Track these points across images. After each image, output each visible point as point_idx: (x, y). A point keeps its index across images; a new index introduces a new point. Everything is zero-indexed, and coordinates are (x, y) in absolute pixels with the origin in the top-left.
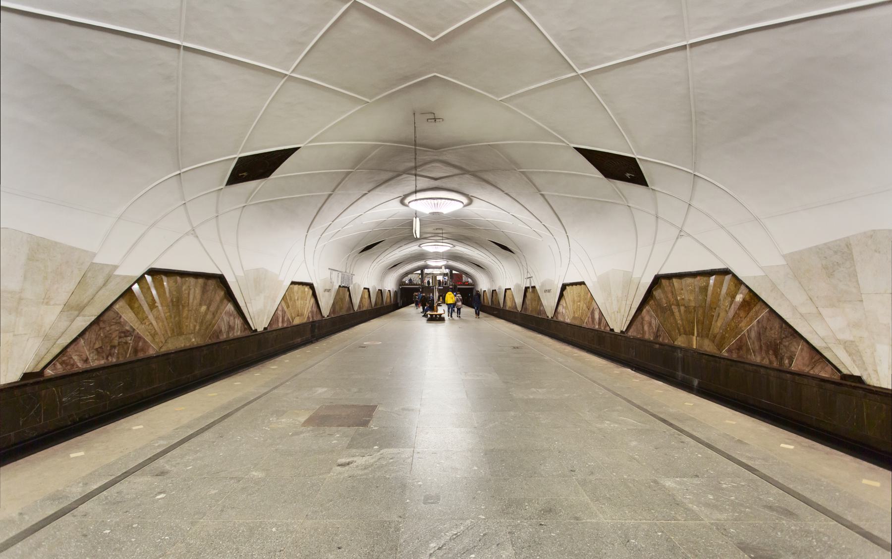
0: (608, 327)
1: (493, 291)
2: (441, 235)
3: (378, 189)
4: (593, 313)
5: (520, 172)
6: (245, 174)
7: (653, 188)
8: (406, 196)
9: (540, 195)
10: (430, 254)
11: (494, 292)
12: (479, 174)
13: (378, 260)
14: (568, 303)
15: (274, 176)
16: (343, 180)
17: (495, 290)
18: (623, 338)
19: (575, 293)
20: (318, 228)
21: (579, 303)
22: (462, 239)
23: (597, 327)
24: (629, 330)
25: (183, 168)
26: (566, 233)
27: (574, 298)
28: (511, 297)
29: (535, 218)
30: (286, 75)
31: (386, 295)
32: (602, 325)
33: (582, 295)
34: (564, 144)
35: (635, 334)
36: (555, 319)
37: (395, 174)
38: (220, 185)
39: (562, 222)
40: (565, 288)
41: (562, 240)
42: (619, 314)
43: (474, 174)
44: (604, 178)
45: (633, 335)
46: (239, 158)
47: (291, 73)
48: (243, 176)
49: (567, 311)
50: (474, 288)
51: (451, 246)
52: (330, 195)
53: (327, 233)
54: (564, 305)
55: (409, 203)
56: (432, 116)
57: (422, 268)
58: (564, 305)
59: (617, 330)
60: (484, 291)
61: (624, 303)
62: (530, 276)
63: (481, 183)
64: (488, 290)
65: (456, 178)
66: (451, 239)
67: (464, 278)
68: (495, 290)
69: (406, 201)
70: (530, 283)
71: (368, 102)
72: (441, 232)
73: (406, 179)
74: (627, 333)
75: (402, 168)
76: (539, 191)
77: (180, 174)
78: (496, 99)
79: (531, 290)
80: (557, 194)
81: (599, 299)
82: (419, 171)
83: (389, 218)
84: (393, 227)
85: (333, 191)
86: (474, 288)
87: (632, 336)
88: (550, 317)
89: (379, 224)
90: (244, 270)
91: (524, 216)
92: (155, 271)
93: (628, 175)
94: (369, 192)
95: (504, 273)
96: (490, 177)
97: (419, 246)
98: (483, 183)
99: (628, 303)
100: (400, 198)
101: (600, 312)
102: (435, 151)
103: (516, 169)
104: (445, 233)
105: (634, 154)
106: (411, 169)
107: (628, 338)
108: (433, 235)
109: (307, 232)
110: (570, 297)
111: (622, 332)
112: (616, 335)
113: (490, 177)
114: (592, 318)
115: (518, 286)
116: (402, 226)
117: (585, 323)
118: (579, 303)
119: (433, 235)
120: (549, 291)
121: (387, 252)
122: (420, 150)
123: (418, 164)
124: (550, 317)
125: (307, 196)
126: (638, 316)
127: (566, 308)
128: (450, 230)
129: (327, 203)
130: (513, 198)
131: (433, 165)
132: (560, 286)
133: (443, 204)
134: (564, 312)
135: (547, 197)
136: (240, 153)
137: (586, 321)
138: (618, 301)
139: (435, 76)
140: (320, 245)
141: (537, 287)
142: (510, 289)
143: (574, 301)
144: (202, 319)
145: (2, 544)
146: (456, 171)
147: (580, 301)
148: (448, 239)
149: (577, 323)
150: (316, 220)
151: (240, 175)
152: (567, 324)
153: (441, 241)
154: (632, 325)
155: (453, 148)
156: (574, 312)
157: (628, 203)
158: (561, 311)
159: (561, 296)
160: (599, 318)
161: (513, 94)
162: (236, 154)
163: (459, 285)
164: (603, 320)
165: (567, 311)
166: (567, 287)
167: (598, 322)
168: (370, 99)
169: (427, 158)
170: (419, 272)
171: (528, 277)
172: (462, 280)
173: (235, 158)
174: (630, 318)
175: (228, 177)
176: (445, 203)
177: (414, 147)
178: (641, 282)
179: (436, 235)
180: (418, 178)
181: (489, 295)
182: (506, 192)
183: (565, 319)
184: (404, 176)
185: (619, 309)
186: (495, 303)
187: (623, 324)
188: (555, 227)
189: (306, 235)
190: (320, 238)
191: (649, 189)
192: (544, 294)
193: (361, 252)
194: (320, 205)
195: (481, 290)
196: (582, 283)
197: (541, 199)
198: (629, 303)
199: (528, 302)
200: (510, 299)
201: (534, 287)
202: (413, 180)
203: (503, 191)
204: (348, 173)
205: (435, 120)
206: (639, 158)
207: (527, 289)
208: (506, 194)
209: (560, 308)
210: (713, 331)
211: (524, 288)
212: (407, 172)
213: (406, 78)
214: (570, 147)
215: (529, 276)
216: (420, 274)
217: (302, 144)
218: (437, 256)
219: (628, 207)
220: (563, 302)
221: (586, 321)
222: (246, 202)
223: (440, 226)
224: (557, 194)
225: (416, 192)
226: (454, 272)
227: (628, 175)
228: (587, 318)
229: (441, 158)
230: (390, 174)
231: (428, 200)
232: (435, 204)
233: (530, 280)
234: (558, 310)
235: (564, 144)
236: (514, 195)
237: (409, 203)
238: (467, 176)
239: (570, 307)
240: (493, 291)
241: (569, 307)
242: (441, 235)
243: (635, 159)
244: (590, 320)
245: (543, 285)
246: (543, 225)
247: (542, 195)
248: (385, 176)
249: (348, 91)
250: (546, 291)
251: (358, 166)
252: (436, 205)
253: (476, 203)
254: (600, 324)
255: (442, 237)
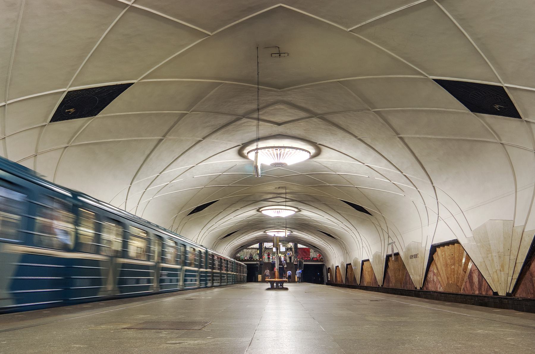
0: (491, 291)
1: (347, 265)
2: (284, 196)
3: (214, 136)
4: (471, 276)
5: (374, 111)
6: (72, 110)
7: (527, 119)
8: (245, 145)
9: (398, 139)
10: (271, 221)
11: (349, 266)
12: (329, 117)
13: (209, 226)
14: (439, 267)
15: (99, 115)
16: (176, 123)
17: (350, 264)
18: (510, 302)
19: (447, 255)
20: (143, 180)
21: (453, 267)
22: (308, 201)
23: (477, 292)
24: (517, 290)
25: (8, 100)
26: (432, 184)
27: (446, 261)
28: (370, 270)
29: (394, 168)
30: (127, 5)
31: (94, 227)
32: (483, 289)
33: (456, 256)
34: (422, 77)
35: (524, 295)
36: (425, 289)
37: (234, 118)
38: (43, 122)
39: (427, 170)
40: (435, 251)
41: (430, 200)
42: (502, 273)
43: (322, 117)
44: (471, 112)
45: (521, 296)
46: (69, 92)
47: (132, 4)
48: (69, 112)
49: (439, 278)
50: (324, 265)
51: (296, 210)
52: (161, 140)
53: (150, 188)
54: (435, 271)
55: (248, 153)
56: (276, 51)
57: (261, 241)
58: (435, 271)
59: (502, 293)
60: (337, 267)
61: (507, 258)
62: (392, 241)
63: (330, 127)
64: (342, 265)
65: (302, 123)
66: (296, 201)
67: (313, 254)
68: (350, 264)
69: (245, 152)
70: (393, 250)
71: (210, 35)
72: (284, 191)
73: (245, 124)
74: (514, 296)
75: (241, 111)
76: (397, 134)
77: (5, 105)
78: (346, 29)
79: (393, 258)
80: (418, 136)
81: (477, 257)
82: (262, 114)
83: (224, 173)
84: (228, 184)
85: (164, 136)
86: (324, 265)
87: (521, 298)
88: (418, 288)
89: (213, 179)
90: (472, 230)
91: (382, 166)
92: (458, 28)
93: (497, 107)
94: (204, 138)
95: (360, 240)
96: (339, 119)
97: (258, 211)
98: (334, 128)
99: (512, 257)
100: (238, 148)
101: (480, 274)
102: (279, 90)
103: (370, 109)
104: (289, 193)
105: (500, 82)
106: (253, 111)
107: (517, 300)
108: (275, 195)
109: (131, 184)
110: (441, 260)
111: (508, 294)
112: (501, 298)
113: (339, 119)
114: (470, 282)
115: (377, 257)
116: (238, 183)
117: (462, 289)
118: (453, 267)
119: (275, 195)
120: (416, 256)
121: (220, 216)
122: (263, 89)
123: (261, 106)
124: (418, 288)
125: (135, 140)
126: (526, 272)
127: (438, 274)
128: (296, 189)
129: (156, 150)
130: (352, 225)
131: (277, 107)
132: (429, 248)
133: (287, 154)
134: (435, 280)
135: (406, 141)
136: (70, 87)
137: (463, 287)
138: (500, 257)
139: (281, 6)
140: (144, 201)
141: (402, 254)
142: (368, 260)
143: (446, 265)
144: (258, 130)
145: (434, 1)
146: (303, 114)
147: (454, 264)
148: (292, 200)
149: (451, 291)
150: (141, 170)
151: (67, 111)
152: (440, 293)
153: (284, 204)
154: (520, 285)
155: (299, 86)
156: (448, 278)
157: (501, 140)
158: (431, 279)
159: (431, 260)
160: (479, 281)
161: (364, 23)
162: (66, 88)
163: (306, 261)
164: (484, 283)
165: (439, 278)
166: (437, 249)
167: (477, 286)
168: (212, 32)
169: (270, 99)
170: (257, 246)
171: (390, 242)
172: (309, 255)
173: (64, 91)
174: (516, 276)
175: (505, 90)
176: (289, 153)
177: (257, 86)
178: (525, 231)
179: (278, 195)
180: (261, 123)
181: (342, 271)
182: (359, 137)
183: (437, 288)
184: (244, 120)
185: (502, 266)
186: (350, 280)
187: (509, 285)
188: (418, 176)
189: (130, 187)
190: (130, 187)
191: (522, 121)
192: (410, 260)
193: (188, 215)
194: (147, 152)
195: (333, 266)
196: (455, 242)
197: (401, 144)
198: (513, 257)
199: (390, 273)
200: (368, 272)
201: (397, 254)
202: (254, 126)
203: (356, 137)
204: (183, 115)
205: (280, 55)
206: (506, 87)
207: (388, 257)
208: (360, 139)
209: (430, 275)
210: (506, 296)
211: (385, 257)
212: (247, 115)
213: (251, 10)
214: (428, 79)
215: (390, 241)
216: (257, 249)
217: (136, 79)
218: (279, 223)
219: (501, 145)
220: (433, 268)
221: (463, 287)
222: (68, 143)
223: (283, 183)
224: (418, 136)
225: (258, 139)
226: (300, 246)
227: (497, 107)
228: (464, 284)
229: (285, 99)
230: (229, 118)
231: (270, 150)
232: (277, 211)
233: (392, 246)
234: (428, 279)
235: (422, 77)
236: (368, 141)
237: (248, 153)
238: (315, 119)
239: (443, 273)
240: (347, 265)
241: (441, 272)
242: (284, 196)
243: (502, 87)
244: (468, 285)
245: (408, 249)
246: (405, 175)
247: (401, 138)
248: (222, 120)
249: (190, 23)
250: (412, 257)
251: (192, 109)
252: (278, 212)
253: (325, 150)
254: (480, 289)
255: (286, 198)
